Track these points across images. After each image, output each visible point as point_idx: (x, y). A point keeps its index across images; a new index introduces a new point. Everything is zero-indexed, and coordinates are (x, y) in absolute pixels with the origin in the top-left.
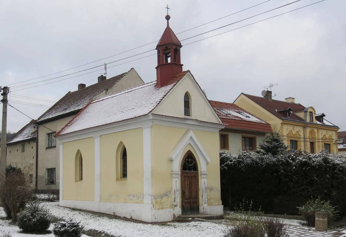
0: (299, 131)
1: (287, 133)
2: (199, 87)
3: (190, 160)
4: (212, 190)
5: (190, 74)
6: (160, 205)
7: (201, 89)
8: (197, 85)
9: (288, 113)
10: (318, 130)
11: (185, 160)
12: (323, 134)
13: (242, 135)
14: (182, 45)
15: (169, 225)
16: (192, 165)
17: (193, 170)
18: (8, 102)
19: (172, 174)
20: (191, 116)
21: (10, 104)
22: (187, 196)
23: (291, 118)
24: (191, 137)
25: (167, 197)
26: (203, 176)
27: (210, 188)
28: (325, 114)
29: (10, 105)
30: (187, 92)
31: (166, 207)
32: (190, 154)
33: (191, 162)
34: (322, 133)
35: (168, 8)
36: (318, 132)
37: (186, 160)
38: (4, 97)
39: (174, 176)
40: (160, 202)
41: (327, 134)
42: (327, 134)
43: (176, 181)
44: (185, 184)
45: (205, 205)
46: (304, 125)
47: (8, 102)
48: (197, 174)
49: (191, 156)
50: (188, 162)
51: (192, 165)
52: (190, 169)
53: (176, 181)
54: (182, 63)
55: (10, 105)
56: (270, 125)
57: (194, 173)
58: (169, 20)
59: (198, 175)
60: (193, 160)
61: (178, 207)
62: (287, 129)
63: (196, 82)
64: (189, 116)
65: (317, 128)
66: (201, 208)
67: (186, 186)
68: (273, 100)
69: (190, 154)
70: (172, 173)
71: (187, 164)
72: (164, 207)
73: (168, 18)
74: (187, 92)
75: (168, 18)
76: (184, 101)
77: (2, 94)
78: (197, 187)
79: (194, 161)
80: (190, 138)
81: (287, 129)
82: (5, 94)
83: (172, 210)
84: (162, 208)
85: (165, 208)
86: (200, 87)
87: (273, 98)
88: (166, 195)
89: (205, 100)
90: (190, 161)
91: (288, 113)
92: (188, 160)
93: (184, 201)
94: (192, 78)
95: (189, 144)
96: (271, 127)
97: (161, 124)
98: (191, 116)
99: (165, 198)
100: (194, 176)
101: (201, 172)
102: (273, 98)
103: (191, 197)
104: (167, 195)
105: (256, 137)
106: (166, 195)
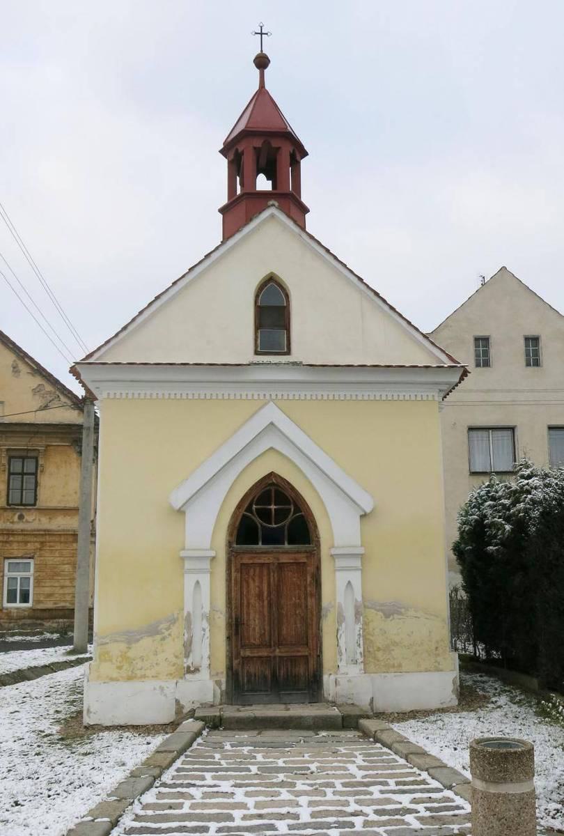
2: (323, 252)
3: (273, 507)
4: (400, 613)
6: (120, 668)
7: (341, 263)
9: (238, 178)
15: (366, 734)
16: (287, 522)
17: (289, 544)
19: (183, 559)
22: (257, 636)
25: (158, 637)
26: (340, 563)
27: (382, 605)
31: (148, 673)
33: (281, 515)
39: (188, 565)
40: (124, 657)
43: (198, 582)
44: (248, 592)
45: (355, 671)
48: (315, 555)
49: (276, 491)
50: (264, 515)
51: (287, 522)
52: (272, 538)
53: (198, 582)
57: (298, 552)
58: (266, 71)
59: (319, 560)
61: (204, 674)
66: (328, 680)
67: (252, 601)
70: (182, 554)
71: (258, 521)
72: (139, 673)
73: (262, 62)
75: (262, 62)
78: (311, 602)
79: (297, 509)
83: (170, 685)
84: (130, 678)
85: (144, 676)
88: (153, 631)
89: (361, 291)
91: (238, 178)
92: (259, 507)
93: (238, 654)
97: (148, 393)
99: (146, 642)
100: (298, 564)
104: (158, 633)
106: (153, 631)
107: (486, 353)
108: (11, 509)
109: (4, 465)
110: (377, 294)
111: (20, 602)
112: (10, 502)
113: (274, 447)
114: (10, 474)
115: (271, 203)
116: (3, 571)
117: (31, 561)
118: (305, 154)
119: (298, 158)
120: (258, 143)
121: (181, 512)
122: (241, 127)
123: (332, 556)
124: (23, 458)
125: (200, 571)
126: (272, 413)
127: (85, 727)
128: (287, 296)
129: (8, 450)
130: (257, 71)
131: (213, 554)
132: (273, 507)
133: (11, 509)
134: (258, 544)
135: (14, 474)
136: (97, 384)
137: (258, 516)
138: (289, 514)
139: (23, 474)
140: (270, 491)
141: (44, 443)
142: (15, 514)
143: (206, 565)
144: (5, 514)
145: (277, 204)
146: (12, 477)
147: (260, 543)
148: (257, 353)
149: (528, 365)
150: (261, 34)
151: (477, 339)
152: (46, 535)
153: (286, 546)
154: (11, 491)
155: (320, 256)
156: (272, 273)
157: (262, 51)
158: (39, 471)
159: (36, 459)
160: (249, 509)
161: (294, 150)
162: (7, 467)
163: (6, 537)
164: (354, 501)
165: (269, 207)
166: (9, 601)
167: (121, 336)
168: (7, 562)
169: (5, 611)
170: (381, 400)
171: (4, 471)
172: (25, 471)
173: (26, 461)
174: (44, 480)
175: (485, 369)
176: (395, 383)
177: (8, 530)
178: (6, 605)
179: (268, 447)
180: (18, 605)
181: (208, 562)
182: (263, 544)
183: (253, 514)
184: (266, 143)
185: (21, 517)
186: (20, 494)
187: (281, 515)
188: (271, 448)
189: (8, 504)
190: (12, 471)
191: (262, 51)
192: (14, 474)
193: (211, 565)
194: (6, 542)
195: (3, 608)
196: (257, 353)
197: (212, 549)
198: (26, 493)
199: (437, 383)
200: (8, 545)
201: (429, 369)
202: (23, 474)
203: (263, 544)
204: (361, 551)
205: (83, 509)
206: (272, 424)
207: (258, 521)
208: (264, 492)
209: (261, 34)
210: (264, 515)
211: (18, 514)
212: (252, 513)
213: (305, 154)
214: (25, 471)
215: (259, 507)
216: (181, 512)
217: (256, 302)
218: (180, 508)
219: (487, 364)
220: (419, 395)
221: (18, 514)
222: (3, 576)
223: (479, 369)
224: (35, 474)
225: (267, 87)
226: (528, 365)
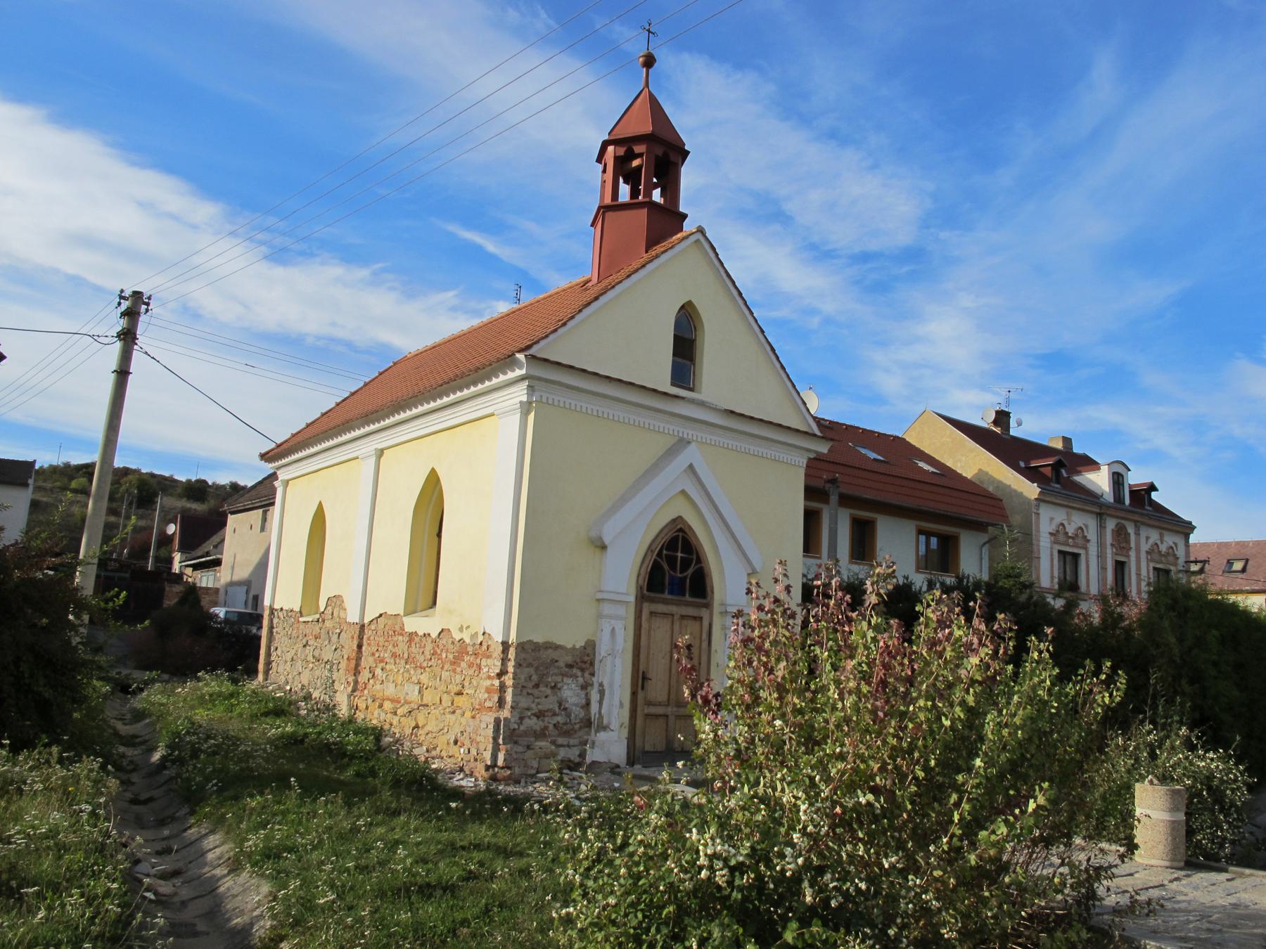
0: (1084, 529)
1: (1051, 531)
2: (735, 293)
3: (679, 554)
5: (702, 240)
8: (729, 284)
10: (1136, 526)
11: (661, 550)
12: (1151, 541)
13: (917, 526)
14: (686, 148)
16: (690, 571)
18: (137, 341)
20: (700, 393)
21: (146, 348)
23: (1064, 487)
24: (691, 467)
28: (1157, 485)
29: (146, 353)
30: (690, 303)
32: (681, 534)
33: (686, 564)
34: (1147, 538)
35: (649, 31)
36: (1137, 534)
37: (665, 552)
38: (129, 323)
41: (1162, 543)
42: (1162, 543)
46: (1098, 511)
47: (137, 341)
49: (683, 537)
51: (690, 571)
54: (682, 209)
55: (146, 353)
56: (1001, 500)
60: (695, 557)
62: (1052, 519)
63: (726, 272)
64: (692, 390)
65: (1135, 522)
68: (1013, 437)
69: (681, 530)
70: (599, 596)
71: (666, 567)
74: (690, 303)
76: (676, 337)
77: (123, 314)
79: (699, 560)
80: (685, 471)
81: (1052, 519)
82: (132, 315)
86: (740, 294)
87: (1012, 433)
90: (681, 557)
92: (669, 553)
94: (712, 255)
95: (683, 492)
96: (1002, 508)
98: (700, 393)
101: (722, 604)
102: (1012, 433)
103: (672, 696)
105: (959, 534)
110: (773, 350)
113: (686, 490)
125: (617, 618)
127: (532, 666)
132: (679, 554)
138: (690, 565)
153: (688, 598)
160: (660, 554)
184: (666, 154)
201: (436, 539)
205: (220, 576)
208: (692, 549)
210: (672, 561)
212: (661, 558)
215: (669, 553)
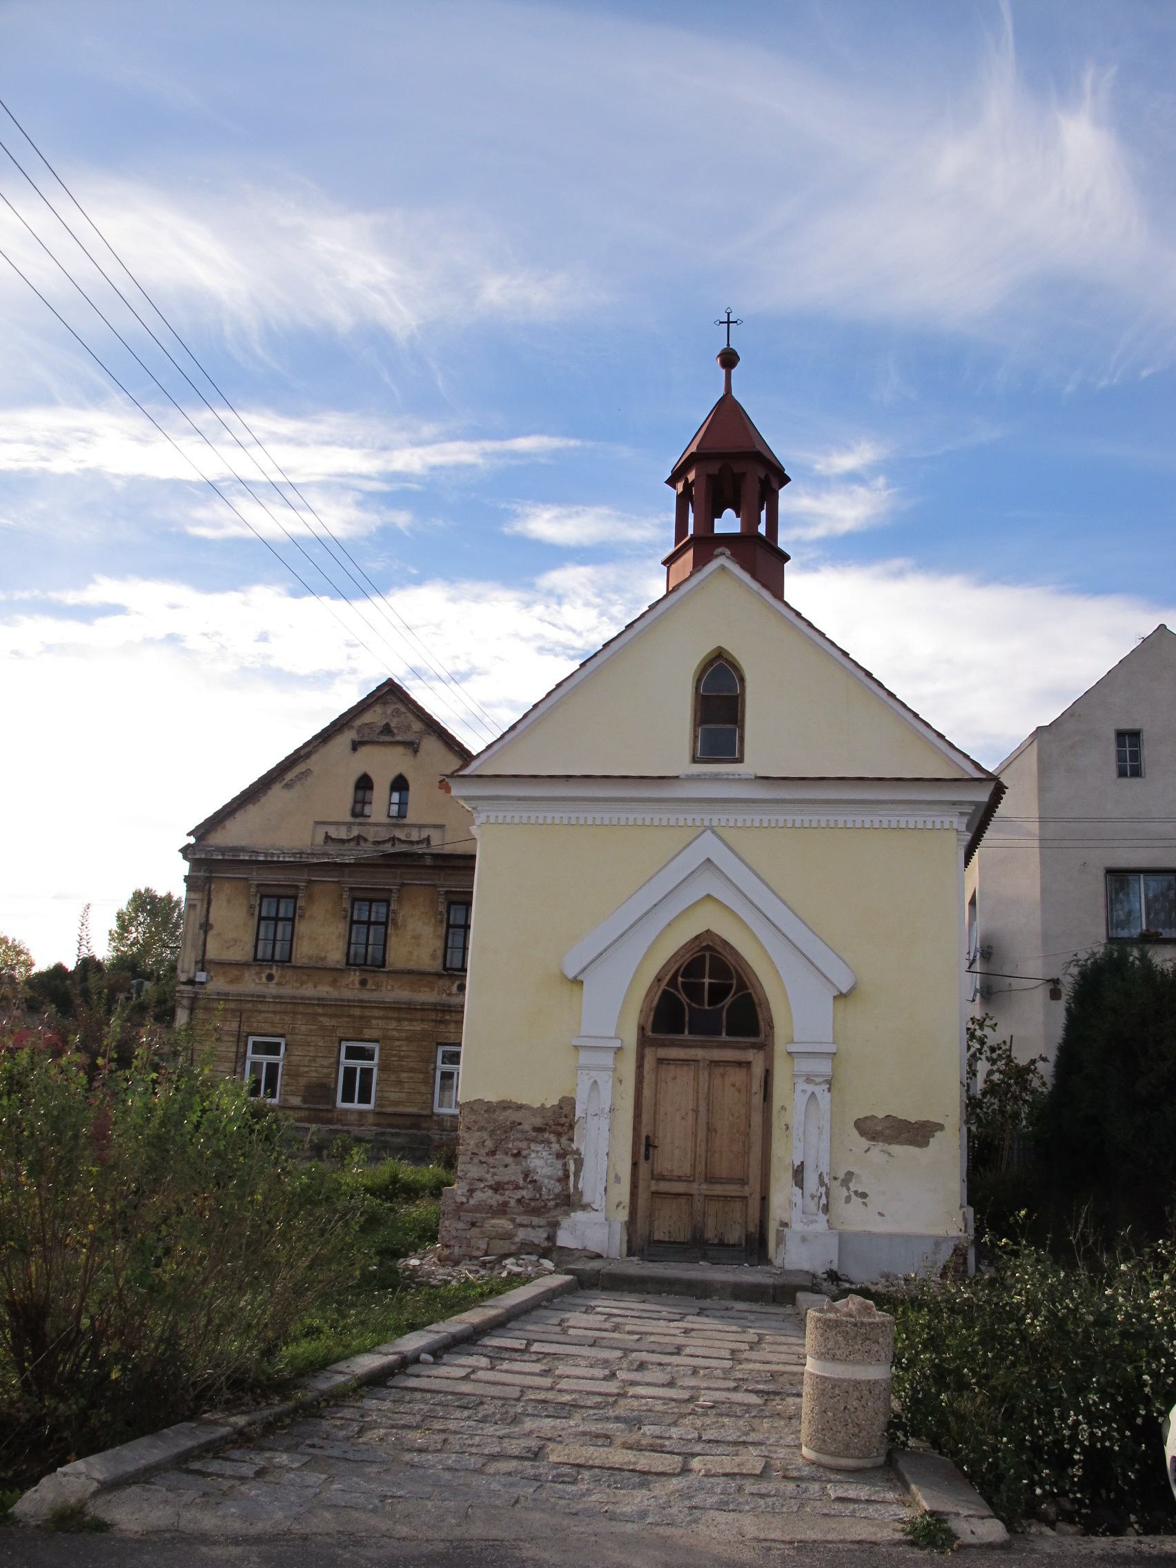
2: (792, 616)
3: (707, 981)
9: (763, 514)
16: (728, 1001)
33: (718, 993)
58: (733, 371)
71: (683, 998)
73: (729, 359)
75: (729, 359)
79: (742, 985)
107: (1136, 756)
108: (448, 975)
109: (441, 913)
111: (359, 1102)
112: (448, 966)
114: (449, 926)
115: (719, 550)
116: (435, 1063)
117: (282, 1041)
118: (785, 480)
119: (775, 485)
120: (714, 468)
121: (577, 982)
122: (693, 449)
123: (789, 1053)
124: (279, 898)
126: (708, 846)
128: (742, 680)
129: (447, 892)
130: (723, 371)
131: (617, 1044)
133: (448, 975)
134: (683, 1032)
135: (381, 923)
136: (474, 803)
137: (684, 990)
139: (369, 923)
140: (703, 957)
141: (305, 877)
142: (453, 983)
143: (608, 1059)
144: (441, 982)
145: (728, 552)
146: (451, 931)
147: (724, 1034)
148: (695, 760)
149: (1122, 773)
150: (728, 322)
151: (1121, 735)
152: (220, 1000)
154: (449, 951)
155: (793, 626)
156: (720, 648)
157: (728, 345)
158: (297, 917)
159: (388, 902)
160: (673, 982)
161: (767, 476)
162: (446, 916)
163: (440, 1015)
164: (825, 977)
165: (717, 556)
166: (344, 1100)
167: (508, 738)
168: (441, 1050)
169: (435, 1118)
170: (761, 827)
171: (345, 918)
172: (373, 919)
173: (453, 907)
174: (302, 927)
175: (1133, 780)
176: (519, 799)
177: (443, 1005)
178: (340, 1104)
179: (705, 894)
180: (356, 1106)
181: (612, 1055)
182: (690, 1033)
183: (678, 991)
185: (363, 983)
186: (461, 955)
187: (718, 993)
188: (708, 896)
189: (445, 968)
190: (355, 918)
191: (728, 345)
192: (381, 923)
193: (615, 1058)
194: (441, 1022)
195: (433, 1113)
196: (695, 760)
197: (616, 1037)
198: (452, 952)
199: (954, 803)
200: (442, 1026)
202: (277, 919)
203: (690, 1033)
204: (833, 1049)
206: (708, 860)
207: (683, 998)
209: (728, 322)
211: (458, 983)
212: (675, 987)
213: (785, 480)
214: (373, 919)
216: (577, 982)
217: (697, 688)
218: (576, 977)
219: (1136, 772)
220: (930, 820)
221: (458, 983)
222: (435, 1069)
223: (1124, 780)
224: (292, 920)
225: (734, 394)
226: (1122, 773)
